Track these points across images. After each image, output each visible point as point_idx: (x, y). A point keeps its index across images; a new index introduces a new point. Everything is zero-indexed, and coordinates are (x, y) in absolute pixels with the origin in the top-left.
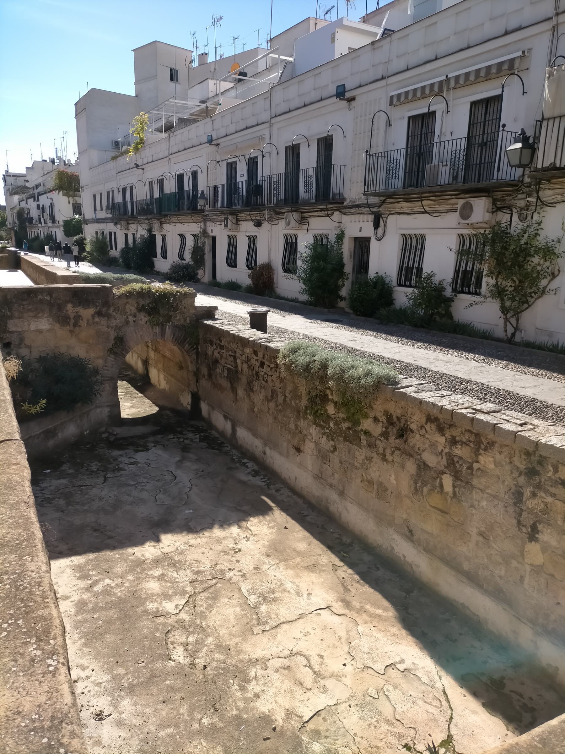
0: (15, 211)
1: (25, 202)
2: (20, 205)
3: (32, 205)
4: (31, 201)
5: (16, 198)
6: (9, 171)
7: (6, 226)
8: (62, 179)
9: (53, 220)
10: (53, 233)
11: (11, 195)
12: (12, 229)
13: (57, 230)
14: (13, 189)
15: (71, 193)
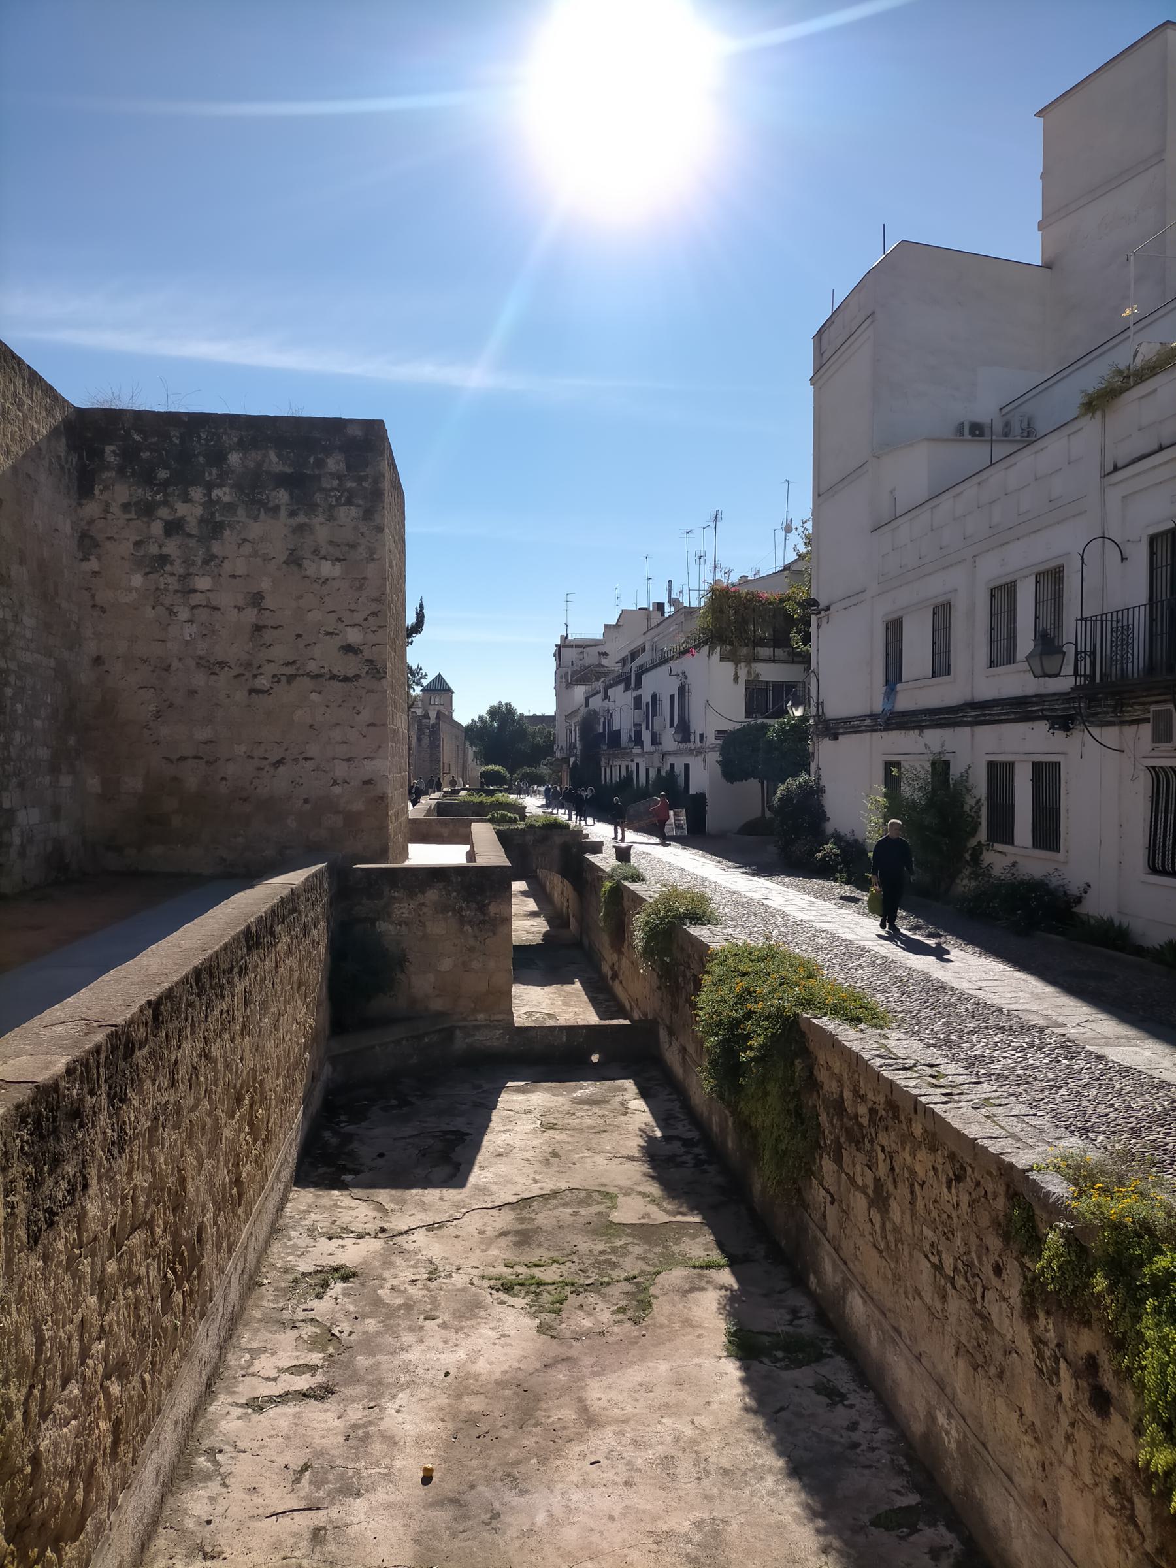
0: (578, 718)
2: (587, 705)
3: (621, 698)
4: (617, 692)
5: (580, 692)
7: (552, 753)
8: (722, 612)
9: (684, 730)
10: (679, 769)
11: (569, 685)
12: (566, 760)
14: (574, 673)
15: (744, 651)
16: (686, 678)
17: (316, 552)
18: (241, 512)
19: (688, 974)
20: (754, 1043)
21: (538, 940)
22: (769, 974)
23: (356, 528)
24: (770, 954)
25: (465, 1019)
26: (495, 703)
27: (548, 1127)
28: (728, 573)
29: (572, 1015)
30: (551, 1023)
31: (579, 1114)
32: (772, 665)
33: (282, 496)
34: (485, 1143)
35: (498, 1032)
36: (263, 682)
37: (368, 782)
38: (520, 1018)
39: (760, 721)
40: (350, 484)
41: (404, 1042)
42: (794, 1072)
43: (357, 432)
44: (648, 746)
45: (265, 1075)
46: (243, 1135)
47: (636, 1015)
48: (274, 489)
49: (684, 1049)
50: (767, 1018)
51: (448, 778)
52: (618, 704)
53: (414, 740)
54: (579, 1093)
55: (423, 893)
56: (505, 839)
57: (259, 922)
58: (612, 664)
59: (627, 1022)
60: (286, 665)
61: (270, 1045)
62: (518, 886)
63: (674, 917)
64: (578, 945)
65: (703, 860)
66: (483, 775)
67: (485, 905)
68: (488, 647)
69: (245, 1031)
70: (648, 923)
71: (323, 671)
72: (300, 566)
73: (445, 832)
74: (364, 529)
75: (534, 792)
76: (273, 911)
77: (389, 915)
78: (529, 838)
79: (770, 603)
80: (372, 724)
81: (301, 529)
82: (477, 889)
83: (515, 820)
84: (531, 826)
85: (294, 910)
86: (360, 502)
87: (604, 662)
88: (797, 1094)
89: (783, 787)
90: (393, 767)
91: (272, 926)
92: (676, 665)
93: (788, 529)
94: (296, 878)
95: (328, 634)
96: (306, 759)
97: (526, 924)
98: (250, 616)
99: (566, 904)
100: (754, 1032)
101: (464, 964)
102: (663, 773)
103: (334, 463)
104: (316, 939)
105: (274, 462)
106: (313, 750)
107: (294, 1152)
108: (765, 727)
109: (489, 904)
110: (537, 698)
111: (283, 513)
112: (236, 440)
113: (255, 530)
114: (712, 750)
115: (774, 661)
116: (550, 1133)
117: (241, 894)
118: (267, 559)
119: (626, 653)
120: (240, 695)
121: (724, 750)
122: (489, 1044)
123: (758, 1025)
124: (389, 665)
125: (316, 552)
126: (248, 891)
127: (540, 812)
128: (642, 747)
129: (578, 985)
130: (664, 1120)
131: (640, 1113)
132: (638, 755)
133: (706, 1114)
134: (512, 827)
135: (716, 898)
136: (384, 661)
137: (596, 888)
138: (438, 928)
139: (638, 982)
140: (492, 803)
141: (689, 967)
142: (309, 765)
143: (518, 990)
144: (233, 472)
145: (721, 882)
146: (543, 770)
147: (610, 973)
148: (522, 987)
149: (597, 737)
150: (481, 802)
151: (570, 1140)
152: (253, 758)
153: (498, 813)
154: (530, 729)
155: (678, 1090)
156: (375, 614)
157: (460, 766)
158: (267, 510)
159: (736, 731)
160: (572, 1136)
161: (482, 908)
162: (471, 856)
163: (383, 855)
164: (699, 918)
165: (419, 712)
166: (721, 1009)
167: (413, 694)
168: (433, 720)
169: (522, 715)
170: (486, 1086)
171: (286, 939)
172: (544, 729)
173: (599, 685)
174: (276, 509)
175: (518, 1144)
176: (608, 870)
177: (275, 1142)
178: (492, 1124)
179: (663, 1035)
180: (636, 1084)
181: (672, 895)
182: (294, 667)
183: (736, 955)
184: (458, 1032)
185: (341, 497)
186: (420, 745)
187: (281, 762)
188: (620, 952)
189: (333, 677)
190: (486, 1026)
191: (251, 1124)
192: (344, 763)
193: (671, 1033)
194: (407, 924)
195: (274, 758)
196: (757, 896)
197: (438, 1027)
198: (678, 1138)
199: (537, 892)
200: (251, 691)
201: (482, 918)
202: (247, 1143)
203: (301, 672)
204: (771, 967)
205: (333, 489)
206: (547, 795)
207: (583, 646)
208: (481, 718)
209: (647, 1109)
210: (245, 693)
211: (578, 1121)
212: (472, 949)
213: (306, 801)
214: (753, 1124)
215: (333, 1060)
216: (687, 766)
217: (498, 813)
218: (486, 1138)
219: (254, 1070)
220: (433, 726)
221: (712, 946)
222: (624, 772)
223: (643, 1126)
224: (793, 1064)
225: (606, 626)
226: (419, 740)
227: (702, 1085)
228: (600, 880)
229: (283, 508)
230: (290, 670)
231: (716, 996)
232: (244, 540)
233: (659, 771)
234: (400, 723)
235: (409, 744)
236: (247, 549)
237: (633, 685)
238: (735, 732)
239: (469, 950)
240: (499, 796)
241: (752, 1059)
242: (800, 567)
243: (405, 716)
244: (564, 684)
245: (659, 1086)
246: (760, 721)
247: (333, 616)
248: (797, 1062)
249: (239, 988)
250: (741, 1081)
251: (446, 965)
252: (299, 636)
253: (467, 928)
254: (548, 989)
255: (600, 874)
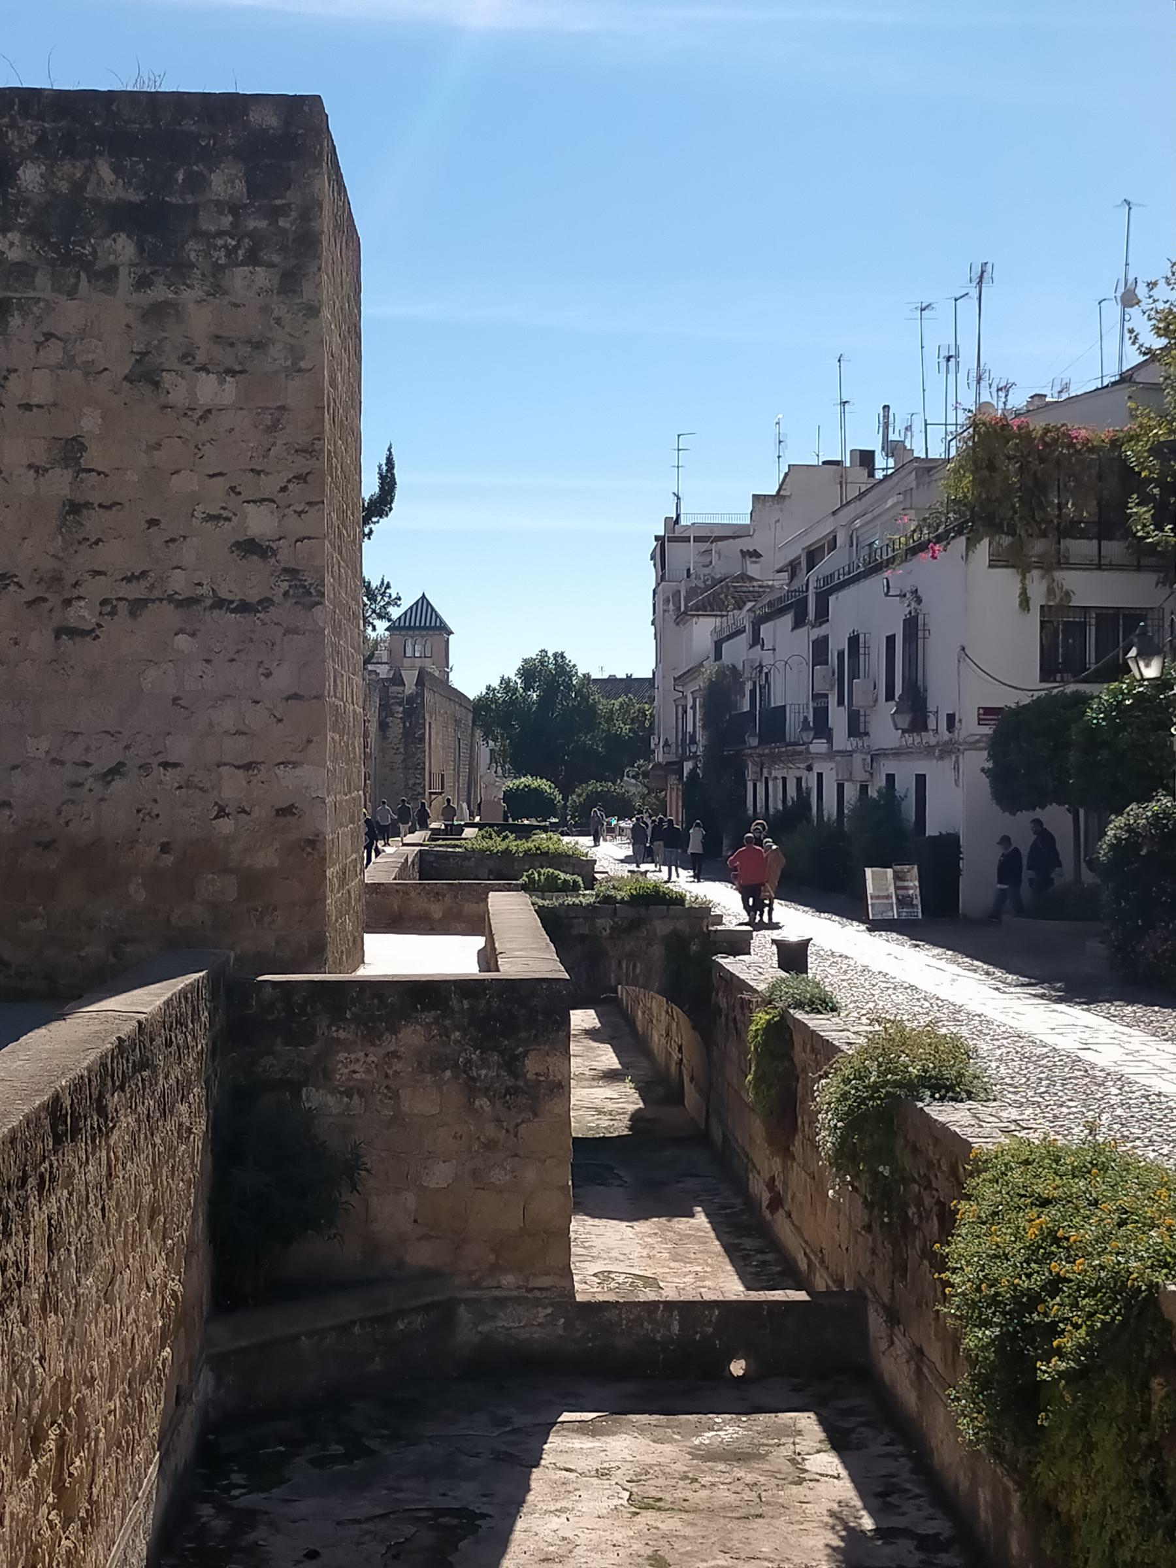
0: (700, 683)
1: (744, 639)
2: (718, 656)
3: (787, 642)
4: (779, 630)
5: (703, 629)
6: (684, 521)
7: (648, 754)
8: (992, 467)
9: (915, 707)
10: (905, 785)
11: (681, 617)
12: (675, 767)
13: (938, 774)
14: (692, 592)
15: (1038, 547)
16: (919, 600)
17: (187, 357)
18: (42, 279)
19: (928, 1201)
20: (1066, 1342)
21: (621, 1127)
22: (1095, 1203)
23: (265, 310)
24: (1097, 1163)
25: (476, 1285)
26: (533, 653)
27: (643, 1505)
28: (1005, 389)
29: (689, 1279)
30: (650, 1295)
31: (706, 1480)
32: (1097, 574)
33: (122, 249)
34: (517, 1536)
35: (543, 1313)
36: (83, 614)
37: (286, 811)
38: (587, 1285)
39: (1071, 688)
40: (256, 223)
41: (357, 1329)
42: (1149, 1404)
43: (272, 121)
44: (841, 738)
45: (85, 1391)
46: (44, 1509)
47: (821, 1283)
48: (107, 235)
49: (920, 1351)
50: (1093, 1292)
51: (438, 803)
52: (782, 654)
53: (373, 728)
54: (707, 1437)
55: (395, 1031)
56: (555, 924)
57: (77, 1087)
58: (768, 574)
59: (802, 1296)
60: (128, 579)
61: (96, 1332)
62: (582, 1019)
63: (896, 1084)
64: (702, 1138)
65: (954, 968)
66: (509, 796)
67: (516, 1058)
68: (521, 542)
69: (49, 1303)
70: (845, 1096)
71: (199, 591)
72: (156, 385)
73: (436, 910)
74: (281, 310)
75: (611, 830)
76: (104, 1065)
77: (327, 1075)
78: (604, 924)
79: (1092, 450)
80: (296, 697)
81: (156, 313)
82: (501, 1025)
83: (575, 887)
84: (608, 900)
85: (144, 1064)
86: (276, 258)
87: (753, 570)
88: (1154, 1449)
89: (1120, 821)
90: (336, 787)
91: (101, 1096)
92: (895, 575)
93: (1129, 300)
94: (146, 1001)
95: (211, 518)
96: (166, 765)
97: (599, 1096)
98: (59, 483)
99: (676, 1056)
100: (1066, 1320)
101: (475, 1174)
102: (873, 793)
103: (225, 182)
104: (186, 1120)
105: (108, 182)
106: (179, 748)
107: (142, 1547)
108: (1082, 700)
109: (525, 1054)
110: (616, 643)
111: (125, 280)
112: (33, 139)
113: (70, 315)
114: (973, 746)
115: (1099, 566)
116: (649, 1517)
117: (42, 1031)
118: (92, 372)
119: (796, 551)
120: (39, 641)
121: (998, 746)
122: (523, 1335)
123: (1075, 1305)
124: (328, 579)
125: (187, 357)
126: (55, 1026)
127: (624, 870)
128: (830, 741)
129: (701, 1220)
130: (877, 1495)
131: (830, 1481)
132: (820, 757)
133: (964, 1484)
134: (570, 900)
135: (983, 1047)
136: (320, 572)
137: (738, 1029)
138: (422, 1101)
139: (824, 1217)
140: (527, 852)
141: (929, 1186)
142: (170, 777)
143: (581, 1227)
144: (27, 202)
145: (991, 1014)
146: (630, 786)
147: (766, 1196)
148: (590, 1221)
149: (736, 722)
150: (507, 851)
151: (688, 1531)
152: (62, 763)
153: (542, 873)
154: (603, 705)
155: (908, 1436)
156: (301, 478)
157: (463, 779)
158: (94, 276)
159: (1021, 710)
160: (692, 1524)
161: (512, 1064)
162: (488, 958)
163: (315, 955)
164: (949, 1088)
165: (383, 671)
166: (996, 1272)
167: (373, 635)
168: (410, 688)
169: (587, 677)
170: (520, 1420)
171: (127, 1121)
172: (630, 704)
173: (743, 617)
174: (111, 273)
175: (584, 1538)
176: (761, 987)
177: (105, 1525)
178: (530, 1498)
179: (876, 1322)
180: (821, 1421)
181: (892, 1040)
182: (144, 584)
183: (1027, 1162)
184: (462, 1310)
185: (236, 248)
186: (385, 738)
187: (116, 771)
188: (787, 1154)
189: (219, 603)
190: (519, 1300)
191: (59, 1488)
192: (240, 772)
193: (893, 1318)
194: (361, 1095)
195: (101, 766)
196: (1067, 1043)
197: (429, 1299)
198: (906, 1533)
199: (618, 1030)
200: (59, 632)
201: (510, 1082)
202: (52, 1526)
203: (156, 594)
204: (1100, 1188)
205: (220, 234)
206: (637, 836)
207: (711, 537)
208: (505, 682)
209: (844, 1473)
210: (49, 635)
211: (704, 1493)
212: (490, 1145)
213: (165, 848)
214: (1063, 1507)
215: (219, 1363)
216: (921, 780)
217: (542, 873)
218: (520, 1524)
219: (65, 1381)
220: (411, 699)
221: (977, 1143)
222: (792, 792)
223: (835, 1507)
224: (1145, 1387)
225: (756, 497)
226: (383, 726)
227: (957, 1426)
228: (746, 1006)
229: (123, 272)
230: (137, 591)
231: (987, 1246)
232: (49, 336)
233: (864, 789)
234: (350, 697)
235: (366, 735)
236: (54, 353)
237: (811, 615)
238: (1020, 711)
239: (485, 1146)
240: (541, 840)
241: (1062, 1374)
242: (1155, 374)
243: (357, 680)
244: (672, 615)
245: (868, 1427)
246: (1071, 688)
247: (221, 484)
248: (1156, 1383)
249: (38, 1217)
250: (1042, 1420)
251: (440, 1175)
252: (153, 523)
253: (482, 1102)
254: (642, 1227)
255: (746, 996)
